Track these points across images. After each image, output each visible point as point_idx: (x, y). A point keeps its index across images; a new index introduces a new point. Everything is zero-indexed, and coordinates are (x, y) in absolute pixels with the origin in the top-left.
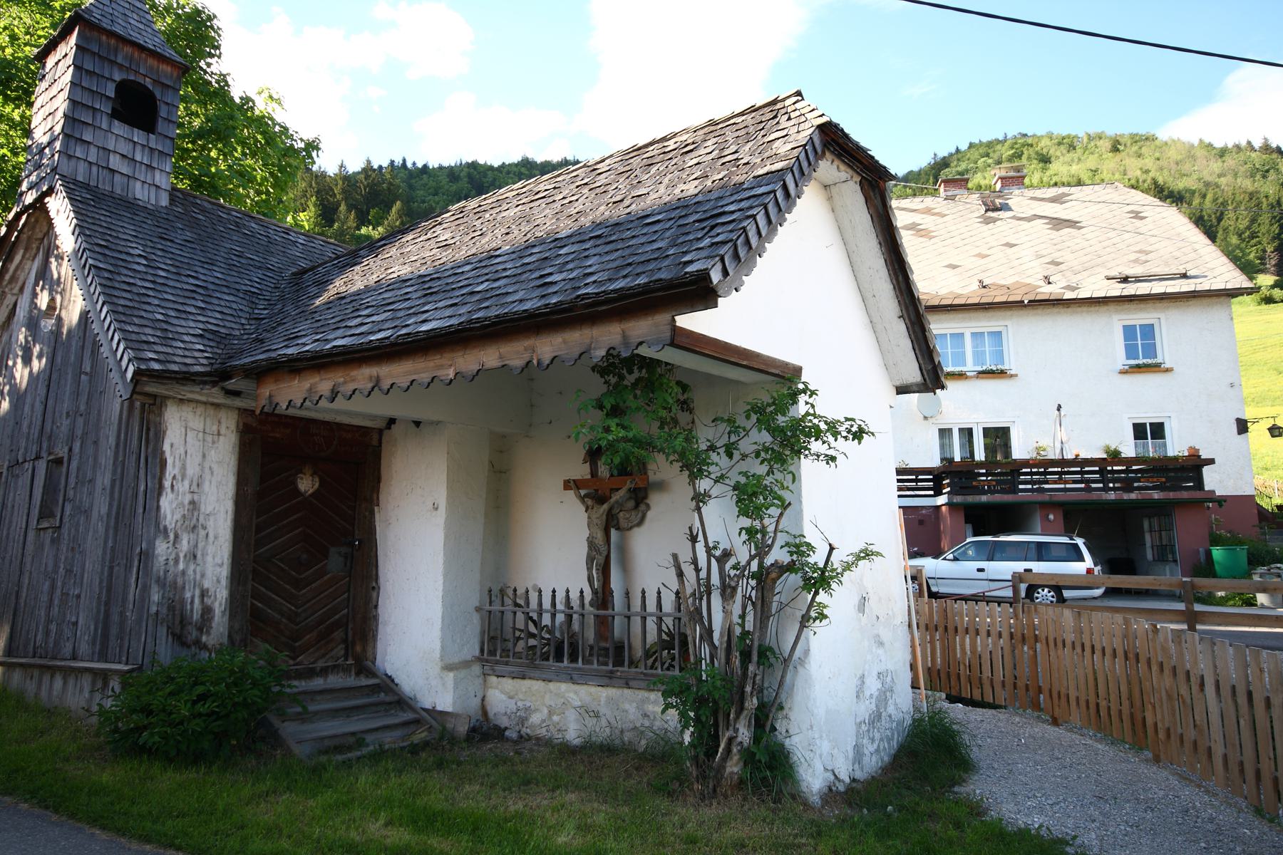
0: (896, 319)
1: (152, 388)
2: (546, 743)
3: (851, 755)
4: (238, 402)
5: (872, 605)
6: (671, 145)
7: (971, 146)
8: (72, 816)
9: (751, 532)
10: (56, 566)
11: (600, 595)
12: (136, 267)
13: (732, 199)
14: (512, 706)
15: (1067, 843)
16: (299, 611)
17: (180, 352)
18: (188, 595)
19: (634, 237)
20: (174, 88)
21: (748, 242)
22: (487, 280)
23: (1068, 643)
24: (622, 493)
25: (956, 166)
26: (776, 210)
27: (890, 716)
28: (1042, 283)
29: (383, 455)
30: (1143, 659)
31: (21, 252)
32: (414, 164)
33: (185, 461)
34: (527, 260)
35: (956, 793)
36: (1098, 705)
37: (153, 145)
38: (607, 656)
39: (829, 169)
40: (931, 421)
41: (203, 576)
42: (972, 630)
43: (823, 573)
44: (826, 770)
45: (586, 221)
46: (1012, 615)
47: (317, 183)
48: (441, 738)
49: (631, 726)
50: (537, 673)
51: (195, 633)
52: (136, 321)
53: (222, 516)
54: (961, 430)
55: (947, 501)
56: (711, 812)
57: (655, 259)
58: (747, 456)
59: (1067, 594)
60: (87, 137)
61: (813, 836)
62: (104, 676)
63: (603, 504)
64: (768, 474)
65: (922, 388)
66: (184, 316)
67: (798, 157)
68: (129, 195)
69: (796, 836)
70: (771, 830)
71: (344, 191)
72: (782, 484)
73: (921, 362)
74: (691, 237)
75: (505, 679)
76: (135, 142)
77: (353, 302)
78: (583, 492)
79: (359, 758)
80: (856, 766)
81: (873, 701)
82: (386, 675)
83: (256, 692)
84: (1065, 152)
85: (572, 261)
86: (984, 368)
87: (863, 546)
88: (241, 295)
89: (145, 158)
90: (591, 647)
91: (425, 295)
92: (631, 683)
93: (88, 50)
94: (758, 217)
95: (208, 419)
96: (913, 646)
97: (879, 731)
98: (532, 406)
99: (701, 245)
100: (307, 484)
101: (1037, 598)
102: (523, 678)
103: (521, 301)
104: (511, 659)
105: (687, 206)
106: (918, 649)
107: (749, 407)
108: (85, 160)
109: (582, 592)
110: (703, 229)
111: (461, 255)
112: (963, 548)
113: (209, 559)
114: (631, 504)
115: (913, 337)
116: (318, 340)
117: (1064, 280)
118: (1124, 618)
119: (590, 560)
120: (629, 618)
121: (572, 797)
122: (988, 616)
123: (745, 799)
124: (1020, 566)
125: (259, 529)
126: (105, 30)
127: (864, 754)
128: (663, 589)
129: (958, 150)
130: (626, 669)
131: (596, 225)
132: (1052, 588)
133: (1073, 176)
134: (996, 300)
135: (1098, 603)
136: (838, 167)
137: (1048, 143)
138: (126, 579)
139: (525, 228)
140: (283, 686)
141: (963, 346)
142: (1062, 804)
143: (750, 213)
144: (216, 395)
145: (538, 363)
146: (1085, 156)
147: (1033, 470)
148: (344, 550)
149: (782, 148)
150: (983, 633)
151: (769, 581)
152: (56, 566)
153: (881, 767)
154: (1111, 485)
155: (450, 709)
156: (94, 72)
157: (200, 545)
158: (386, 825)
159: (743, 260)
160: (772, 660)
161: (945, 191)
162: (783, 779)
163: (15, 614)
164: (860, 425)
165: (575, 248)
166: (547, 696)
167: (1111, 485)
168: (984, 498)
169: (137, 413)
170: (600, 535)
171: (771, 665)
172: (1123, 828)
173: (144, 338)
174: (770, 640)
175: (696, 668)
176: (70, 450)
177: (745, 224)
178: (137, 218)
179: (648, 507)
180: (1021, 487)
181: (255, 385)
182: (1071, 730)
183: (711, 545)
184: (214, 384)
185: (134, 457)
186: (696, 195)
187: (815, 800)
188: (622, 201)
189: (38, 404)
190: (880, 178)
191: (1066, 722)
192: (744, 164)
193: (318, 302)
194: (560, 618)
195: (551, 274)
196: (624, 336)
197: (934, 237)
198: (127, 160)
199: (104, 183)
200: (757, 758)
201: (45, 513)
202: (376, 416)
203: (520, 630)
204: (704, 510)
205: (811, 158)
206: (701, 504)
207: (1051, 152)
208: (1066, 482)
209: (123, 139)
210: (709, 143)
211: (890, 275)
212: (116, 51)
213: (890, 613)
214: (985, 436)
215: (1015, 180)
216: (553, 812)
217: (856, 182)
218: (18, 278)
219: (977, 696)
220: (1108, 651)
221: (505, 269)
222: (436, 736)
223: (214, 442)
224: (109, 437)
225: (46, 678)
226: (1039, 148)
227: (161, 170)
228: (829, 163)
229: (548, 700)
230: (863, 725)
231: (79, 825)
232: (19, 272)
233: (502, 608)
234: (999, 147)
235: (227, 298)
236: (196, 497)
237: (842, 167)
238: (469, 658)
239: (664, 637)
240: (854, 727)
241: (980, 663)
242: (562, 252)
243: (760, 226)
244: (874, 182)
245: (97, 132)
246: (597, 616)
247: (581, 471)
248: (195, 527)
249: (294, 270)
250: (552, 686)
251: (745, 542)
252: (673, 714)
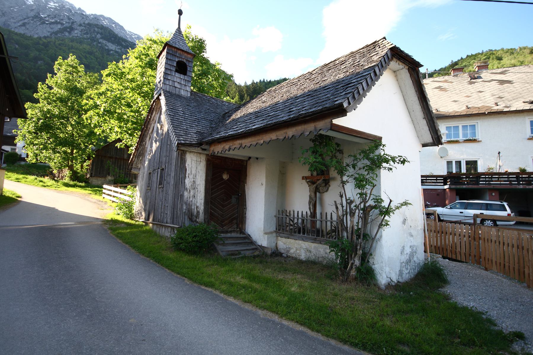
0: (422, 119)
1: (182, 148)
2: (295, 259)
3: (398, 273)
4: (205, 152)
5: (409, 222)
6: (337, 62)
7: (468, 56)
8: (162, 265)
9: (361, 194)
10: (163, 198)
11: (313, 214)
12: (180, 114)
13: (355, 78)
14: (285, 247)
15: (483, 314)
16: (224, 214)
17: (190, 138)
18: (193, 207)
19: (320, 94)
21: (359, 92)
22: (274, 112)
23: (493, 241)
24: (320, 181)
25: (461, 65)
26: (371, 80)
27: (415, 261)
28: (494, 105)
29: (248, 168)
30: (525, 249)
31: (155, 112)
32: (267, 80)
33: (191, 169)
34: (286, 104)
35: (440, 291)
36: (504, 264)
37: (186, 79)
38: (314, 233)
39: (394, 64)
40: (443, 158)
41: (197, 202)
42: (453, 234)
43: (387, 209)
44: (387, 277)
45: (306, 90)
46: (470, 229)
47: (238, 89)
48: (263, 254)
49: (322, 256)
50: (292, 237)
51: (195, 218)
52: (179, 129)
53: (202, 185)
54: (456, 162)
55: (448, 187)
56: (344, 287)
57: (326, 101)
58: (361, 169)
59: (498, 223)
60: (169, 78)
61: (379, 299)
62: (173, 228)
63: (314, 184)
64: (367, 175)
65: (433, 144)
66: (192, 127)
67: (381, 60)
69: (373, 298)
70: (365, 295)
71: (246, 91)
72: (373, 178)
73: (432, 134)
74: (339, 92)
75: (283, 238)
77: (236, 121)
78: (308, 180)
79: (238, 258)
80: (400, 277)
81: (408, 255)
82: (248, 234)
83: (209, 236)
84: (509, 55)
85: (300, 103)
86: (467, 139)
87: (404, 201)
88: (208, 121)
90: (310, 230)
91: (256, 117)
92: (322, 242)
94: (363, 83)
95: (198, 157)
96: (425, 237)
97: (410, 266)
98: (293, 153)
99: (342, 95)
100: (225, 177)
101: (485, 224)
102: (288, 238)
103: (282, 117)
104: (285, 232)
105: (339, 82)
106: (427, 239)
107: (361, 151)
109: (307, 212)
110: (343, 89)
111: (268, 105)
112: (455, 205)
113: (198, 197)
114: (324, 185)
115: (429, 125)
116: (225, 133)
117: (504, 104)
118: (518, 233)
119: (310, 203)
120: (321, 221)
121: (299, 276)
122: (459, 229)
123: (357, 284)
124: (478, 212)
125: (212, 189)
126: (173, 46)
127: (403, 273)
128: (333, 213)
129: (462, 58)
130: (320, 238)
131: (309, 91)
132: (491, 220)
133: (512, 64)
134: (474, 113)
135: (513, 227)
136: (399, 64)
137: (502, 52)
138: (178, 202)
139: (288, 94)
140: (218, 235)
141: (458, 130)
142: (484, 300)
143: (360, 82)
144: (199, 150)
145: (288, 138)
146: (518, 56)
147: (486, 176)
148: (236, 196)
149: (375, 58)
150: (457, 234)
151: (367, 211)
152: (163, 198)
153: (410, 279)
154: (521, 183)
155: (266, 246)
157: (196, 193)
158: (242, 278)
159: (356, 99)
160: (368, 238)
161: (453, 73)
162: (371, 279)
163: (154, 211)
164: (404, 159)
165: (302, 99)
166: (295, 245)
167: (521, 183)
168: (464, 187)
169: (180, 155)
170: (313, 194)
171: (367, 240)
172: (509, 311)
173: (181, 134)
174: (368, 231)
175: (341, 239)
176: (165, 166)
177: (358, 86)
178: (181, 100)
179: (330, 186)
180: (480, 183)
181: (209, 147)
182: (493, 273)
183: (348, 198)
184: (198, 147)
185: (179, 168)
186: (343, 78)
187: (383, 287)
188: (319, 82)
189: (159, 154)
190: (417, 67)
191: (491, 270)
192: (361, 65)
193: (227, 122)
194: (300, 221)
195: (293, 108)
196: (315, 128)
197: (448, 91)
200: (362, 270)
201: (160, 183)
202: (245, 156)
203: (288, 223)
204: (345, 186)
205: (386, 60)
206: (344, 185)
207: (502, 56)
208: (501, 181)
210: (350, 60)
211: (420, 103)
213: (416, 225)
214: (466, 164)
215: (484, 66)
216: (291, 280)
217: (406, 69)
219: (454, 257)
220: (510, 245)
221: (279, 108)
222: (261, 253)
223: (199, 164)
224: (174, 162)
225: (161, 228)
226: (497, 55)
228: (395, 62)
229: (296, 246)
230: (403, 264)
231: (163, 267)
233: (282, 216)
234: (480, 56)
236: (195, 180)
237: (400, 63)
238: (272, 231)
239: (333, 228)
240: (400, 264)
241: (456, 246)
242: (297, 101)
243: (364, 86)
244: (414, 68)
246: (311, 220)
247: (308, 174)
248: (194, 188)
249: (224, 113)
250: (297, 241)
251: (359, 198)
252: (333, 253)
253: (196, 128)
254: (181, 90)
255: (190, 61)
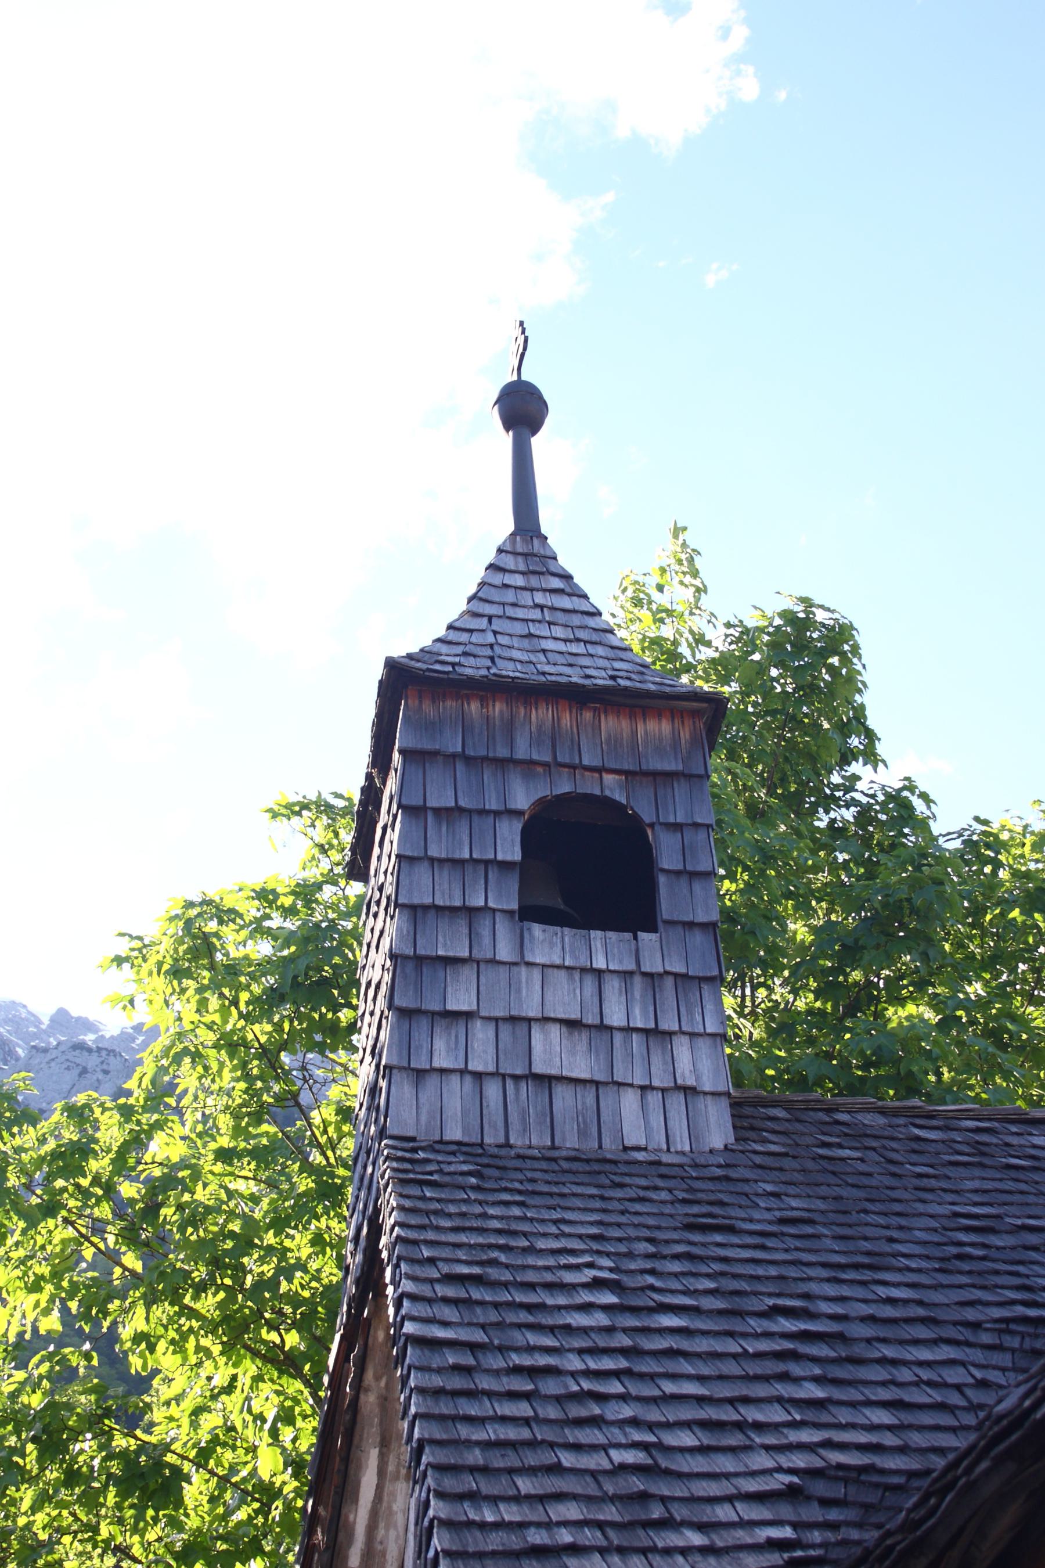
20: (689, 777)
37: (653, 964)
60: (460, 999)
66: (734, 1439)
68: (607, 1143)
76: (599, 972)
89: (637, 1011)
93: (434, 754)
108: (463, 1072)
156: (460, 809)
198: (585, 1034)
199: (525, 1129)
209: (562, 974)
212: (510, 728)
218: (384, 1554)
227: (692, 1035)
232: (381, 1532)
235: (925, 1354)
245: (489, 974)
253: (806, 1436)
254: (608, 1098)
255: (670, 776)
